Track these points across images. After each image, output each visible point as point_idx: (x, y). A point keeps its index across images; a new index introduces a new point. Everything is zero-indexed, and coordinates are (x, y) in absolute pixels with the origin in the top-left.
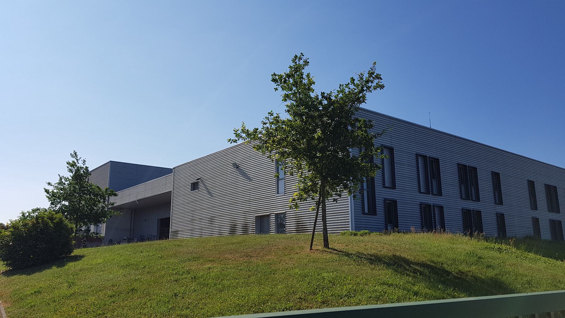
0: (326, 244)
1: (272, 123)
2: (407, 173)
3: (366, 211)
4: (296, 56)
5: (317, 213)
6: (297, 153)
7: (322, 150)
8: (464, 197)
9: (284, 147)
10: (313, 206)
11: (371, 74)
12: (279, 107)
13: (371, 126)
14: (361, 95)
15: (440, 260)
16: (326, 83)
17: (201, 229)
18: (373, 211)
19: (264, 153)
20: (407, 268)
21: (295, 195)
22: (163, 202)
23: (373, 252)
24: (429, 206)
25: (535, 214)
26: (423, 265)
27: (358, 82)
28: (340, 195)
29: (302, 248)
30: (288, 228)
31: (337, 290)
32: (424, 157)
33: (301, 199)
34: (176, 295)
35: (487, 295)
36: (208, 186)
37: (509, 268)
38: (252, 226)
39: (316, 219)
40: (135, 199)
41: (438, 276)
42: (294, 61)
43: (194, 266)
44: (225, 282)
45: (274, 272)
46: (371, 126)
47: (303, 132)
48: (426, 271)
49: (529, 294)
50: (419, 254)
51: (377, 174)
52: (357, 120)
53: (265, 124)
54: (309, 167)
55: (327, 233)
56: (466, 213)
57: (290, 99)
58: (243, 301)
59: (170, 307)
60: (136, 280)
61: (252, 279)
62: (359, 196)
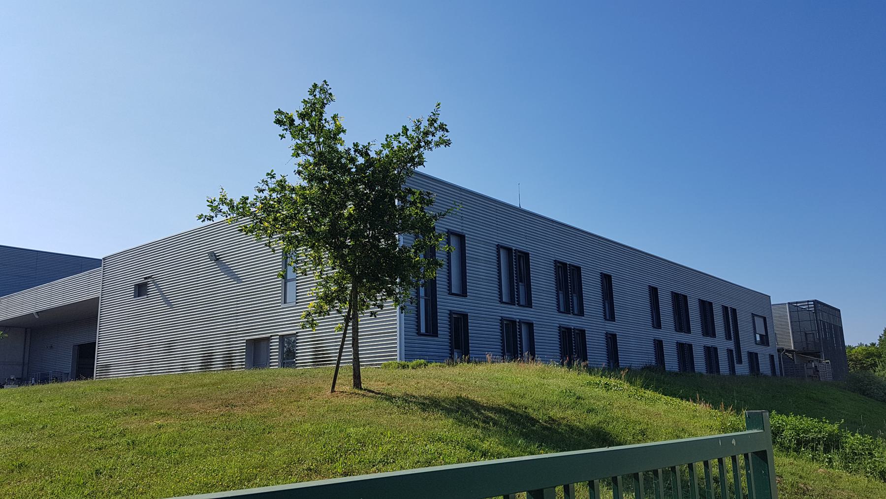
0: (357, 383)
1: (273, 190)
2: (484, 272)
3: (423, 330)
4: (315, 86)
5: (345, 334)
6: (313, 238)
7: (355, 236)
8: (562, 310)
9: (294, 229)
10: (341, 323)
11: (432, 122)
12: (285, 163)
13: (430, 202)
14: (416, 153)
15: (523, 402)
16: (366, 128)
17: (151, 361)
18: (432, 330)
19: (259, 239)
20: (476, 415)
21: (311, 306)
22: (85, 316)
23: (428, 393)
24: (513, 322)
25: (659, 334)
26: (499, 410)
27: (413, 133)
28: (381, 307)
29: (319, 389)
30: (299, 359)
31: (369, 453)
32: (509, 250)
33: (321, 312)
34: (98, 472)
35: (565, 451)
36: (165, 291)
37: (618, 413)
38: (240, 356)
39: (343, 344)
40: (32, 310)
41: (519, 425)
42: (312, 92)
43: (134, 423)
44: (185, 449)
45: (270, 429)
46: (430, 202)
47: (326, 205)
48: (503, 420)
49: (611, 448)
50: (494, 393)
51: (440, 275)
52: (410, 192)
53: (262, 191)
54: (334, 263)
55: (359, 366)
56: (566, 334)
57: (305, 153)
58: (214, 478)
59: (86, 492)
60: (27, 450)
61: (231, 444)
62: (413, 308)
